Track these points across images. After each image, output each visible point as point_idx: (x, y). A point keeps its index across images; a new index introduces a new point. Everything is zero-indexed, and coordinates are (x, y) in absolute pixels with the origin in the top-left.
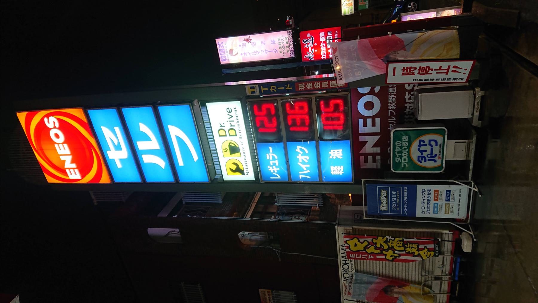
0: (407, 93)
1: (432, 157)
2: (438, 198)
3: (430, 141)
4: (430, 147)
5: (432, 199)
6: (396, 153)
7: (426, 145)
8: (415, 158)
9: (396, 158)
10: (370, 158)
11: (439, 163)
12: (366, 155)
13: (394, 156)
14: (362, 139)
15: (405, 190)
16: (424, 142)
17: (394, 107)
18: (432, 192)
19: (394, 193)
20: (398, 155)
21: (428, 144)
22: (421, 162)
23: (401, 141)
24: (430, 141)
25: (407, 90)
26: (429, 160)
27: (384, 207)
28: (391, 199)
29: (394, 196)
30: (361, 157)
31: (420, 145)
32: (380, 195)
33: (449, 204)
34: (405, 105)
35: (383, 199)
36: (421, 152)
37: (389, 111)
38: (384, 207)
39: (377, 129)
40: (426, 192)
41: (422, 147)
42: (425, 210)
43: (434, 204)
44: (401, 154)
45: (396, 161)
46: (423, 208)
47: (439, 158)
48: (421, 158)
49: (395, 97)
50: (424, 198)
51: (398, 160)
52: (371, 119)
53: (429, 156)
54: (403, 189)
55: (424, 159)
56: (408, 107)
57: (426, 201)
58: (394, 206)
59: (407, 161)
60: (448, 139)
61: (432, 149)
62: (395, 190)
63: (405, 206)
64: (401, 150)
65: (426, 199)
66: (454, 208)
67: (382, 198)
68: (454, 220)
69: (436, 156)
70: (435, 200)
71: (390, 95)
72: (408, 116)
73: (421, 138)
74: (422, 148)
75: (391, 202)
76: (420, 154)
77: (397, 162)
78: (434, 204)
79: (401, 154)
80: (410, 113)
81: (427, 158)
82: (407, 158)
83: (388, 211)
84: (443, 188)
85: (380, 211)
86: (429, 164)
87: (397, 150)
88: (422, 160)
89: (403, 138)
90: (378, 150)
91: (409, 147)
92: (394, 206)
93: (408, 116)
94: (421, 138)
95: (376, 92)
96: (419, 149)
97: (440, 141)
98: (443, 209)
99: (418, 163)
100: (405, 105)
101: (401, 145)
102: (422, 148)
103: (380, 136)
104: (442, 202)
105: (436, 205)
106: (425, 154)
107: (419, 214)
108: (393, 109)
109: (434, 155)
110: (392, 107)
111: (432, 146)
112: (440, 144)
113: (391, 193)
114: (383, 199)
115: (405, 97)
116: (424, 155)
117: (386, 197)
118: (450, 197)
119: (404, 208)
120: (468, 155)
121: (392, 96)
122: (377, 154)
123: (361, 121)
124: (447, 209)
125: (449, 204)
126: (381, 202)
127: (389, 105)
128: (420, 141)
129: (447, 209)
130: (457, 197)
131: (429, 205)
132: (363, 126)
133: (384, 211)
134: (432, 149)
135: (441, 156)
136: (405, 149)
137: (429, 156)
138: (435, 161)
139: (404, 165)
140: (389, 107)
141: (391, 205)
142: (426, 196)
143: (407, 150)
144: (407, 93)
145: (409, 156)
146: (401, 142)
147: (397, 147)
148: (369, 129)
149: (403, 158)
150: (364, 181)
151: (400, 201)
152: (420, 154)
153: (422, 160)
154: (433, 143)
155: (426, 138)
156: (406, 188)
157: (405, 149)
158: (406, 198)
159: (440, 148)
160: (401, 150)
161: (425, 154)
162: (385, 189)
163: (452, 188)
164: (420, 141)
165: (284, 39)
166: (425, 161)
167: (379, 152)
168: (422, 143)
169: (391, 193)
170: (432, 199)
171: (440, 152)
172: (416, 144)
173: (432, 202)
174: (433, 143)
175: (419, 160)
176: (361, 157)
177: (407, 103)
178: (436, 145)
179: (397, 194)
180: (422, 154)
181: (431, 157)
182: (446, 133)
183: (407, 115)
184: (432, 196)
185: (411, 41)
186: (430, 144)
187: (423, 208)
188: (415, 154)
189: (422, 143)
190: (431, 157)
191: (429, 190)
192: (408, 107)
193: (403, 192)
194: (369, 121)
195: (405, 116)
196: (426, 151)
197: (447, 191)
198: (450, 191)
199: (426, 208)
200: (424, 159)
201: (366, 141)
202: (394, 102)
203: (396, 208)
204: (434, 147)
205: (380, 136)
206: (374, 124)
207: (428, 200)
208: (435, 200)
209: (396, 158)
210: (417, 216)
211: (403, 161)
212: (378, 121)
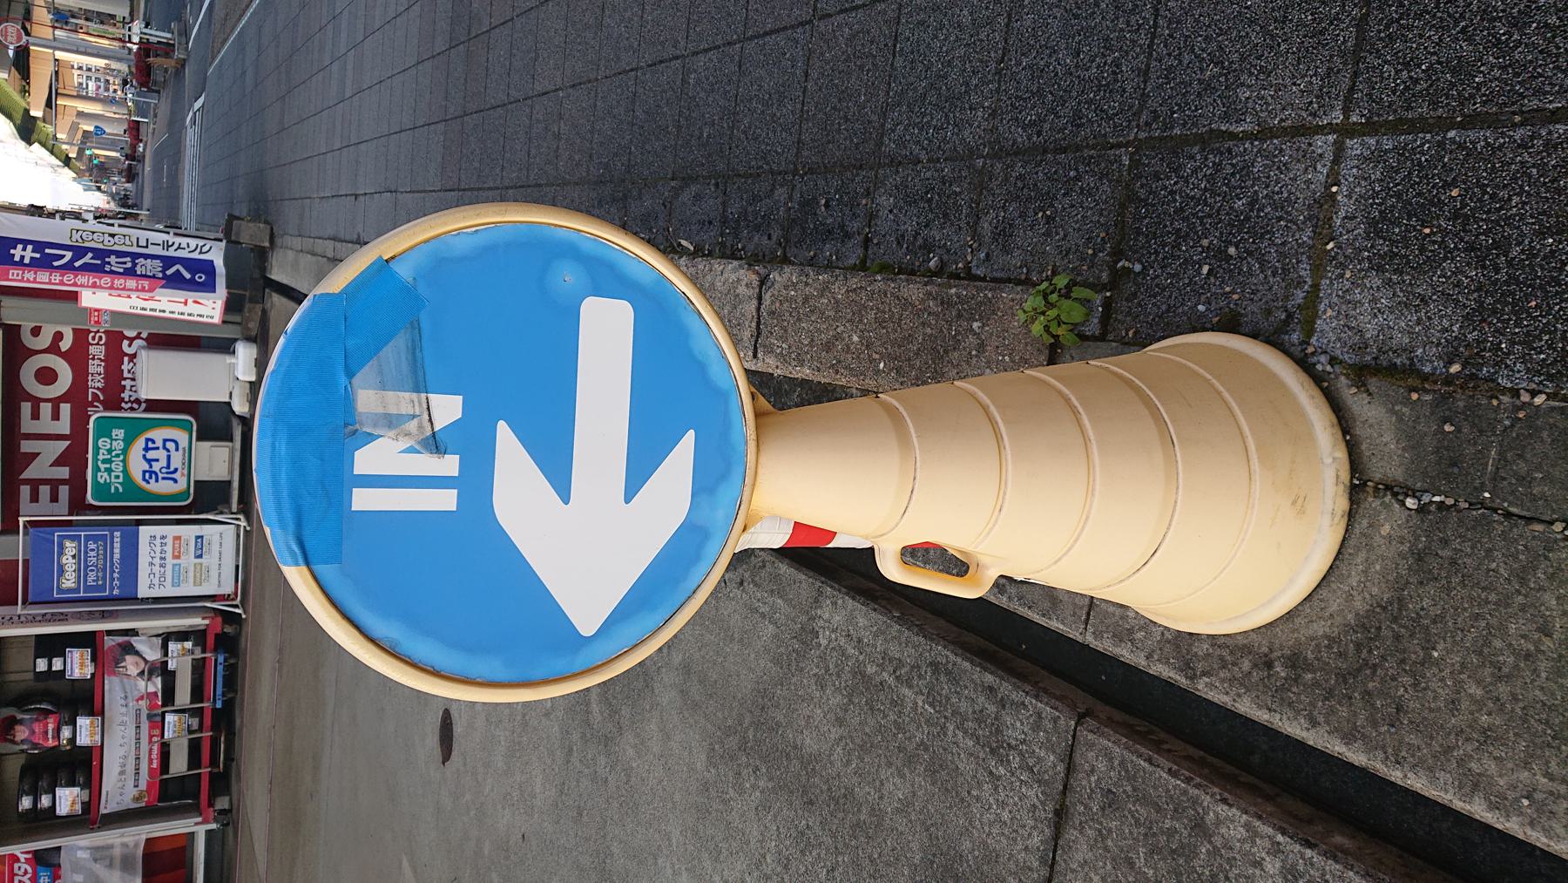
0: (126, 359)
1: (170, 475)
2: (179, 552)
3: (165, 441)
4: (165, 453)
5: (169, 555)
6: (99, 463)
7: (158, 448)
8: (138, 477)
9: (99, 474)
10: (45, 490)
11: (182, 485)
12: (35, 484)
13: (97, 469)
14: (27, 446)
15: (116, 540)
16: (154, 442)
17: (100, 385)
18: (169, 541)
19: (93, 546)
20: (102, 466)
21: (161, 447)
22: (148, 483)
23: (110, 437)
24: (165, 441)
25: (127, 355)
26: (163, 478)
27: (69, 581)
28: (86, 561)
29: (92, 554)
30: (22, 487)
31: (147, 449)
32: (61, 553)
33: (201, 564)
34: (123, 383)
35: (68, 561)
36: (149, 461)
37: (90, 390)
38: (69, 581)
39: (64, 426)
40: (158, 542)
41: (150, 452)
42: (156, 581)
43: (174, 565)
44: (108, 466)
45: (99, 479)
46: (152, 576)
47: (183, 475)
48: (150, 474)
49: (103, 364)
50: (153, 554)
51: (103, 477)
52: (49, 405)
53: (164, 470)
54: (112, 537)
55: (154, 476)
56: (128, 388)
57: (157, 561)
58: (92, 576)
59: (121, 480)
60: (229, 483)
61: (169, 457)
62: (95, 539)
63: (116, 575)
64: (109, 457)
65: (158, 555)
66: (211, 573)
67: (64, 561)
68: (213, 598)
69: (176, 470)
70: (175, 557)
71: (93, 359)
72: (129, 405)
73: (149, 435)
74: (151, 455)
75: (86, 567)
76: (147, 467)
77: (102, 481)
78: (174, 565)
79: (108, 466)
80: (132, 399)
81: (160, 476)
82: (121, 475)
83: (77, 590)
84: (189, 531)
85: (60, 591)
86: (164, 487)
87: (101, 457)
88: (151, 478)
89: (113, 434)
90: (64, 472)
91: (125, 451)
92: (92, 576)
93: (129, 405)
94: (149, 435)
95: (63, 350)
96: (144, 456)
97: (184, 443)
98: (191, 574)
99: (144, 484)
100: (123, 383)
101: (109, 446)
102: (151, 455)
103: (68, 442)
104: (188, 560)
105: (177, 568)
106: (156, 467)
107: (143, 591)
108: (98, 389)
109: (172, 469)
110: (96, 382)
111: (168, 451)
112: (184, 448)
113: (86, 547)
114: (68, 561)
115: (123, 367)
116: (154, 469)
117: (74, 557)
118: (202, 549)
119: (113, 579)
120: (231, 472)
121: (96, 362)
122: (63, 482)
123: (26, 408)
124: (198, 575)
125: (201, 564)
126: (62, 571)
127: (90, 378)
128: (148, 440)
129: (198, 575)
130: (215, 547)
131: (162, 570)
132: (30, 417)
133: (70, 590)
134: (169, 457)
135: (186, 472)
136: (118, 456)
137: (164, 470)
138: (175, 481)
139: (116, 488)
140: (90, 383)
141: (86, 575)
142: (158, 549)
143: (122, 457)
144: (126, 359)
145: (126, 471)
146: (109, 441)
147: (101, 451)
148: (46, 424)
149: (113, 474)
150: (24, 522)
151: (105, 565)
152: (147, 467)
153: (151, 478)
154: (170, 445)
155: (158, 435)
156: (117, 534)
157: (118, 456)
158: (117, 556)
159: (184, 455)
160: (109, 457)
161: (156, 467)
162: (72, 538)
163: (206, 530)
164: (148, 440)
165: (1325, 327)
166: (157, 481)
167: (67, 476)
168: (150, 445)
169: (86, 547)
170: (169, 555)
171: (184, 464)
172: (140, 443)
173: (170, 561)
174: (170, 445)
175: (144, 479)
176: (22, 487)
177: (125, 379)
178: (177, 449)
179: (98, 548)
180: (151, 467)
181: (167, 473)
182: (195, 428)
183: (126, 403)
184: (169, 549)
185: (760, 442)
186: (164, 448)
187: (152, 576)
188: (137, 466)
189: (150, 445)
190: (167, 473)
191: (163, 537)
192: (128, 388)
193: (112, 543)
194: (46, 409)
195: (123, 405)
196: (157, 460)
197: (197, 537)
198: (202, 537)
199: (157, 575)
200: (154, 476)
201: (36, 451)
202: (100, 374)
203: (97, 581)
204: (173, 453)
205: (68, 442)
206: (56, 416)
207: (161, 558)
208: (175, 557)
209: (99, 474)
210: (140, 596)
211: (113, 480)
212: (65, 409)
